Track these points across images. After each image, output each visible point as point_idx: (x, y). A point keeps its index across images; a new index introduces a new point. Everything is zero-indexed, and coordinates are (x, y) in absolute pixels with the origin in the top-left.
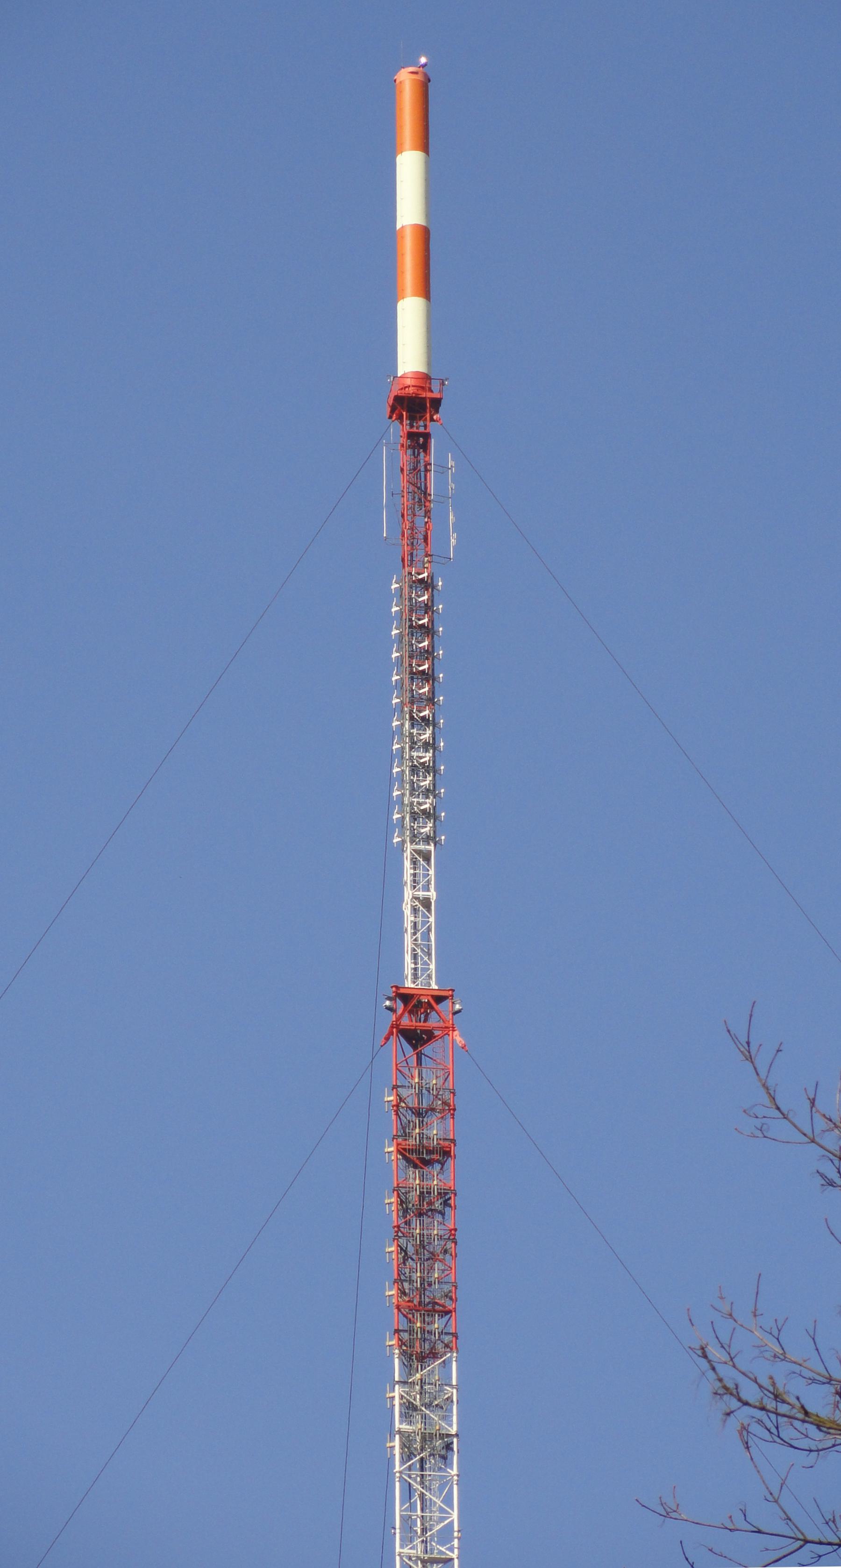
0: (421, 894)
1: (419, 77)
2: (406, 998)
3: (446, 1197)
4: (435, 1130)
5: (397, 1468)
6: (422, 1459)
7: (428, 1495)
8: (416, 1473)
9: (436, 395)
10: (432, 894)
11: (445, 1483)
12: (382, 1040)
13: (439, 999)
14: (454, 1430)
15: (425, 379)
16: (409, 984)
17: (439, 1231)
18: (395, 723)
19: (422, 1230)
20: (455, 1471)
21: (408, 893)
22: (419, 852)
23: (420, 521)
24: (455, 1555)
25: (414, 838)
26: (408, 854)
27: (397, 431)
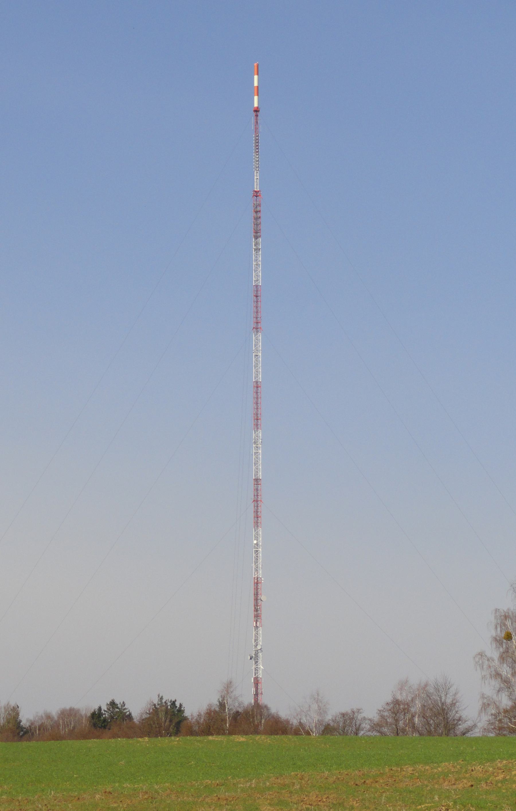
0: (257, 178)
1: (257, 65)
2: (255, 191)
3: (260, 217)
4: (258, 209)
5: (253, 253)
6: (257, 631)
7: (258, 460)
8: (256, 533)
9: (259, 110)
10: (258, 178)
11: (259, 254)
12: (252, 330)
13: (259, 191)
14: (260, 248)
15: (258, 107)
16: (255, 190)
17: (260, 613)
18: (254, 170)
19: (256, 563)
20: (260, 253)
21: (255, 178)
22: (255, 355)
23: (257, 126)
24: (260, 264)
25: (256, 170)
26: (255, 172)
27: (254, 114)
